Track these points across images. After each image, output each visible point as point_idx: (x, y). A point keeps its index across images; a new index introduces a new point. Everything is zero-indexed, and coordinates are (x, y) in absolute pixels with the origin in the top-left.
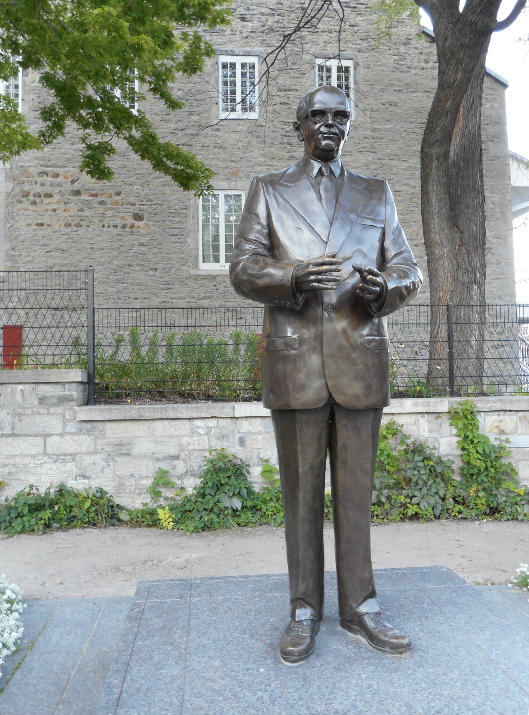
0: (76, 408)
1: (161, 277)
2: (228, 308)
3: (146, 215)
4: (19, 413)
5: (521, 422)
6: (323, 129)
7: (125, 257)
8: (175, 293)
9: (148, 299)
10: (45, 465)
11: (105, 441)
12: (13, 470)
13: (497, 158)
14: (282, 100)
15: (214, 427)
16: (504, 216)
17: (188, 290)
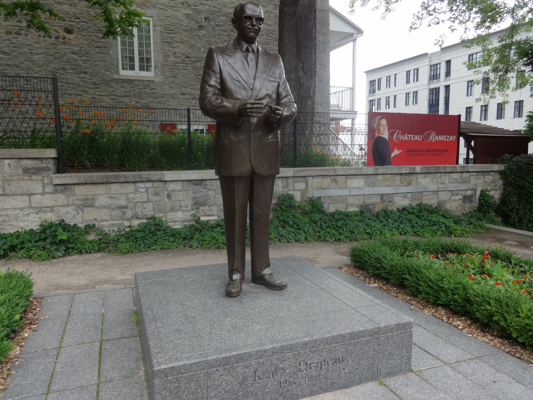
0: (52, 175)
1: (90, 79)
4: (8, 180)
5: (332, 182)
6: (250, 26)
7: (60, 62)
9: (81, 95)
10: (31, 214)
11: (75, 198)
12: (6, 218)
13: (322, 10)
15: (150, 187)
16: (325, 50)
17: (111, 90)
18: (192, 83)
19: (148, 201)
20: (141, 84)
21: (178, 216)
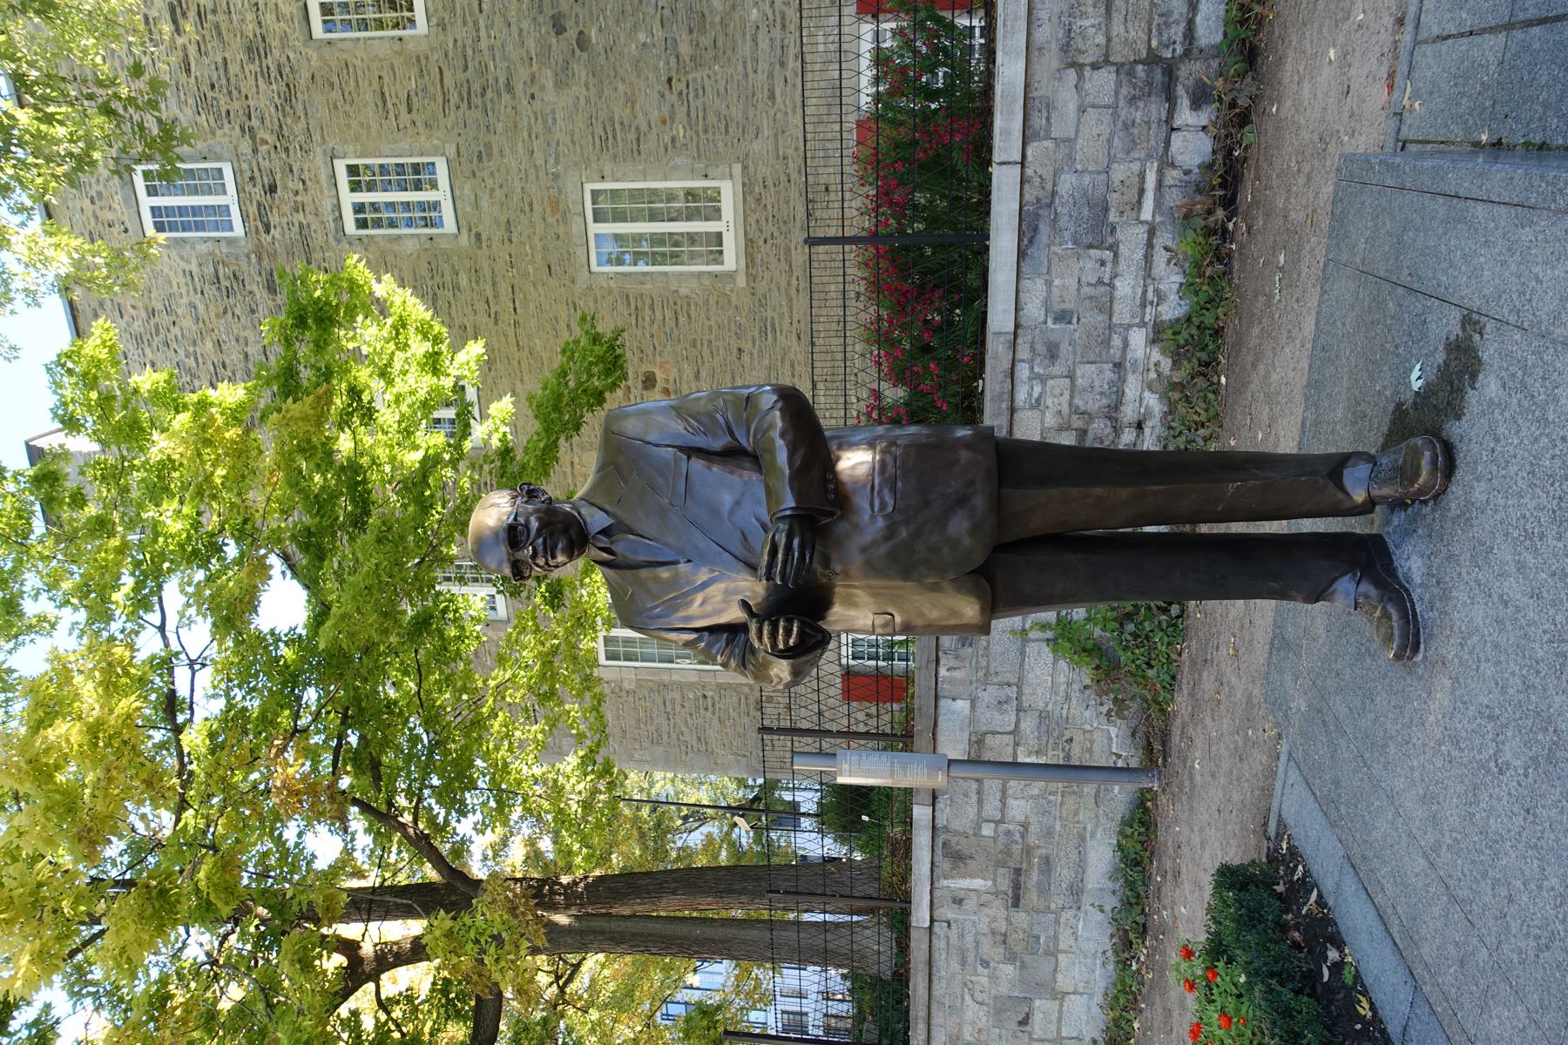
2: (809, 215)
3: (646, 368)
8: (781, 315)
9: (792, 365)
14: (403, 108)
15: (1032, 368)
18: (740, 68)
19: (1071, 377)
20: (755, 217)
21: (1128, 290)
